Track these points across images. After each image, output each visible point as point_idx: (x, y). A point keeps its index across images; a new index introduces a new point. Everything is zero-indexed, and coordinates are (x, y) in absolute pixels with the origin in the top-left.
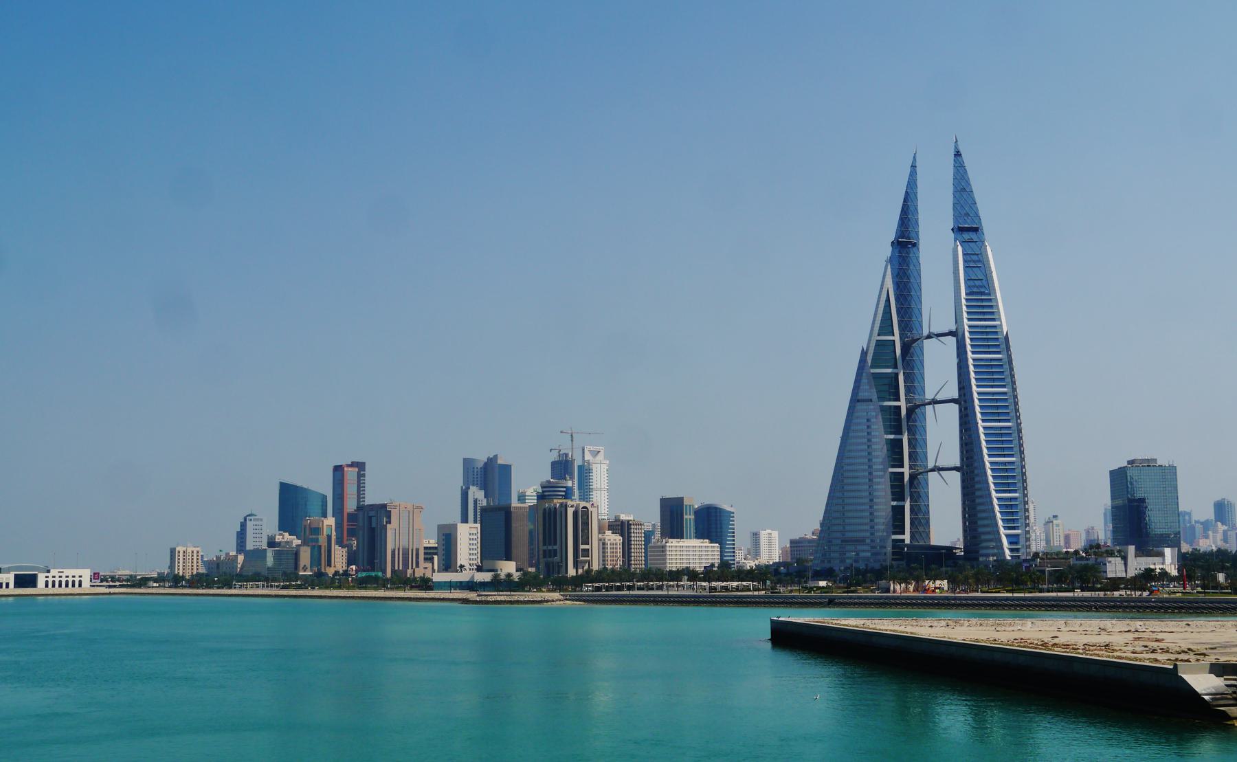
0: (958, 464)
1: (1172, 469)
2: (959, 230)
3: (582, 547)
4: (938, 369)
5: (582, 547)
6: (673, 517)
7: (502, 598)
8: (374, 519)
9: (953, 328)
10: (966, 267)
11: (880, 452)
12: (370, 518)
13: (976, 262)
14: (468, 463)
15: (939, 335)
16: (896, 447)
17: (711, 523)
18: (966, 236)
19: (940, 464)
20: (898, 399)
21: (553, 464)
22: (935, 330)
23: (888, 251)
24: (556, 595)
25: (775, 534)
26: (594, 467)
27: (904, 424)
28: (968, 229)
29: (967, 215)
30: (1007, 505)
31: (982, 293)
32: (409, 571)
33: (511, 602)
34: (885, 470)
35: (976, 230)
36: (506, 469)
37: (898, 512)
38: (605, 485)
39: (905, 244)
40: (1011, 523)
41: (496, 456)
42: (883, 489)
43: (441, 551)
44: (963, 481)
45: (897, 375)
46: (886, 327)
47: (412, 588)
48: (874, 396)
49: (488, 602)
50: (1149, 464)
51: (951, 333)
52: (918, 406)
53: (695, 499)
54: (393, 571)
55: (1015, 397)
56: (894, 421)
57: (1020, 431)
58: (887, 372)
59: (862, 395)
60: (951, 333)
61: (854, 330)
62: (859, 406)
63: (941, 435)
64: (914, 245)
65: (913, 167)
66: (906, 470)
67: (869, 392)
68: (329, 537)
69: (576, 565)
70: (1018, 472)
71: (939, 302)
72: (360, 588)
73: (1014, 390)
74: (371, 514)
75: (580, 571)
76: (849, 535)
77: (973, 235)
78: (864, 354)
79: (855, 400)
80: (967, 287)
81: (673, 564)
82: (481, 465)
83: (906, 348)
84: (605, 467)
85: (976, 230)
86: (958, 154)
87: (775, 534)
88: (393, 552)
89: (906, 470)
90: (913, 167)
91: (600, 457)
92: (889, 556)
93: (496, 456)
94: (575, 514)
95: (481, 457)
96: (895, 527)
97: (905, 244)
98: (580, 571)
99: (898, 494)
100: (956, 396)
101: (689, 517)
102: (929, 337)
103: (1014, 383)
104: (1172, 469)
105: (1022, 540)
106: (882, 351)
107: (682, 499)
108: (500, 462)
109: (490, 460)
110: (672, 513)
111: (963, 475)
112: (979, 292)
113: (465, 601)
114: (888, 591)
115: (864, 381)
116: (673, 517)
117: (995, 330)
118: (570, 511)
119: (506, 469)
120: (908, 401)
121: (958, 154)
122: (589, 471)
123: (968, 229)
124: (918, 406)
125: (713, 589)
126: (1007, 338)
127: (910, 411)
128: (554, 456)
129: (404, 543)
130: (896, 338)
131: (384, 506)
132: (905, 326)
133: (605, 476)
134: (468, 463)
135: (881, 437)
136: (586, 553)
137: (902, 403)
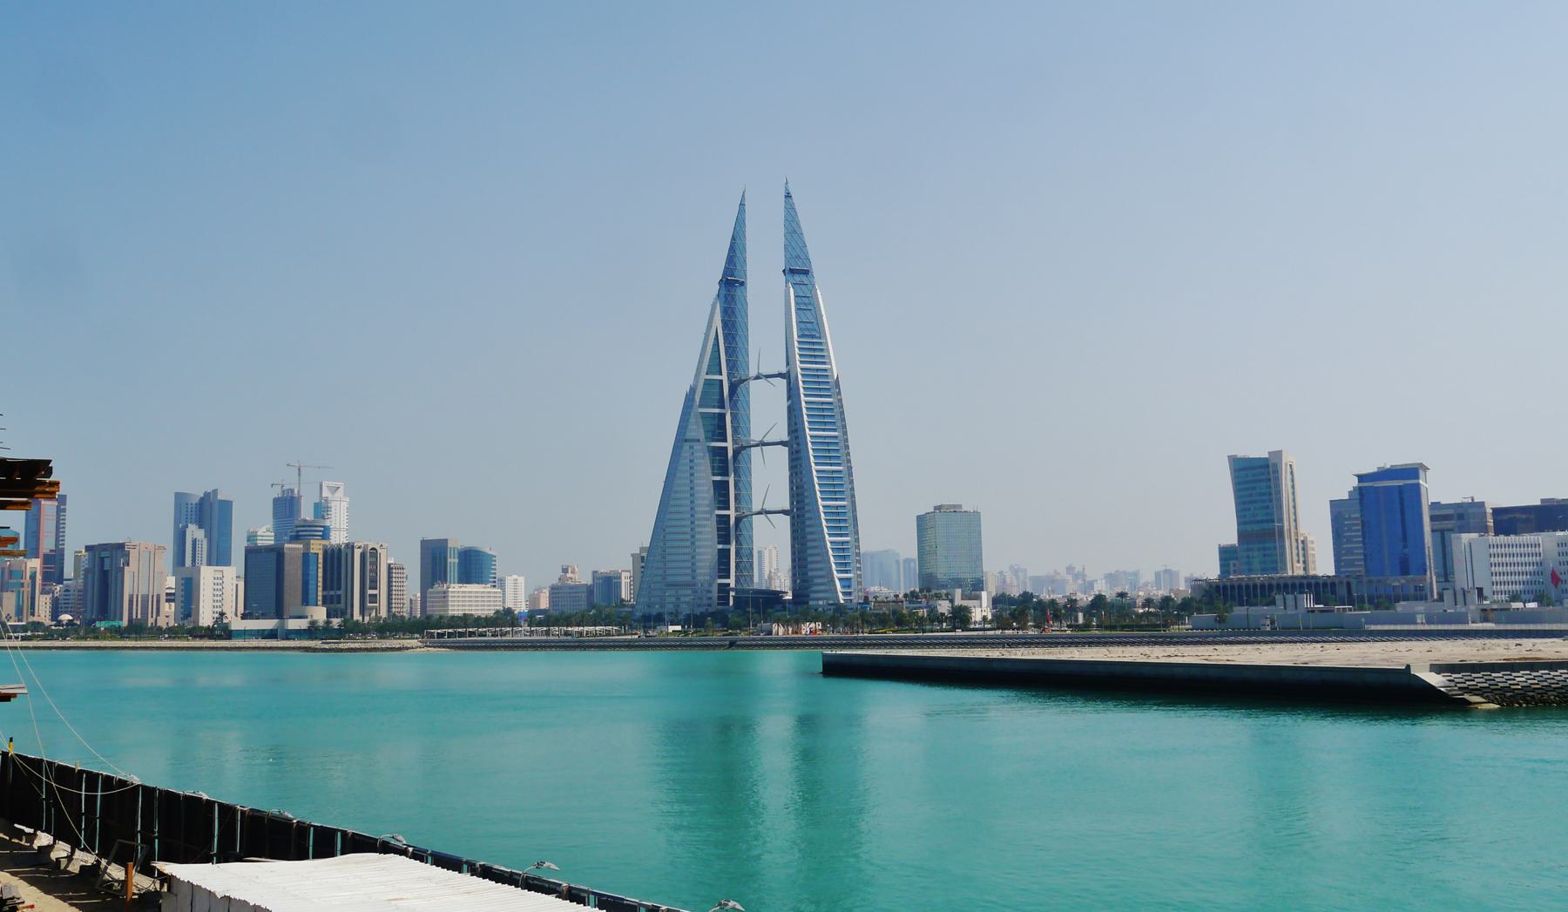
0: (787, 506)
1: (977, 514)
2: (790, 272)
3: (370, 592)
4: (766, 411)
5: (370, 592)
6: (435, 561)
7: (356, 646)
8: (107, 561)
9: (784, 370)
10: (798, 309)
11: (705, 493)
12: (102, 559)
13: (807, 304)
14: (180, 498)
15: (767, 376)
16: (721, 488)
17: (473, 567)
18: (797, 278)
19: (768, 507)
20: (725, 440)
21: (276, 501)
22: (764, 371)
23: (715, 288)
24: (414, 643)
25: (521, 580)
26: (332, 504)
27: (727, 464)
28: (798, 272)
29: (798, 257)
30: (841, 549)
31: (813, 336)
32: (151, 621)
33: (367, 650)
34: (711, 512)
35: (806, 272)
36: (227, 506)
37: (724, 556)
38: (344, 526)
39: (731, 283)
40: (844, 566)
41: (215, 491)
42: (709, 531)
43: (179, 598)
44: (793, 525)
45: (722, 416)
46: (715, 367)
47: (195, 637)
48: (702, 437)
49: (341, 650)
50: (955, 509)
51: (780, 375)
52: (744, 448)
53: (458, 541)
54: (130, 620)
55: (846, 440)
56: (721, 461)
57: (851, 475)
58: (714, 420)
59: (690, 435)
60: (780, 375)
61: (678, 370)
62: (686, 446)
63: (768, 479)
64: (742, 284)
65: (742, 204)
66: (732, 513)
67: (697, 430)
68: (33, 577)
69: (362, 613)
70: (849, 516)
71: (767, 345)
72: (382, 638)
73: (845, 433)
74: (104, 554)
75: (367, 619)
76: (670, 579)
77: (803, 278)
78: (693, 390)
79: (681, 440)
80: (799, 329)
81: (455, 609)
82: (196, 500)
83: (733, 388)
84: (345, 505)
85: (806, 272)
86: (788, 196)
87: (521, 580)
88: (131, 602)
89: (732, 513)
90: (742, 204)
91: (340, 493)
92: (715, 600)
93: (215, 491)
94: (363, 556)
95: (197, 492)
96: (720, 570)
97: (731, 283)
98: (367, 619)
99: (724, 537)
100: (785, 438)
101: (453, 561)
102: (757, 378)
103: (844, 427)
104: (977, 514)
105: (854, 583)
106: (712, 388)
107: (1413, 472)
108: (220, 497)
109: (207, 495)
110: (434, 558)
111: (793, 518)
112: (811, 334)
113: (307, 649)
114: (770, 633)
115: (692, 420)
116: (435, 561)
117: (825, 374)
118: (357, 553)
119: (227, 506)
120: (734, 441)
121: (788, 196)
122: (328, 509)
123: (798, 272)
124: (744, 448)
125: (567, 634)
126: (837, 382)
127: (736, 453)
128: (277, 492)
129: (143, 591)
130: (724, 377)
131: (122, 546)
132: (732, 366)
133: (344, 514)
134: (180, 498)
135: (705, 478)
136: (374, 598)
137: (729, 445)
